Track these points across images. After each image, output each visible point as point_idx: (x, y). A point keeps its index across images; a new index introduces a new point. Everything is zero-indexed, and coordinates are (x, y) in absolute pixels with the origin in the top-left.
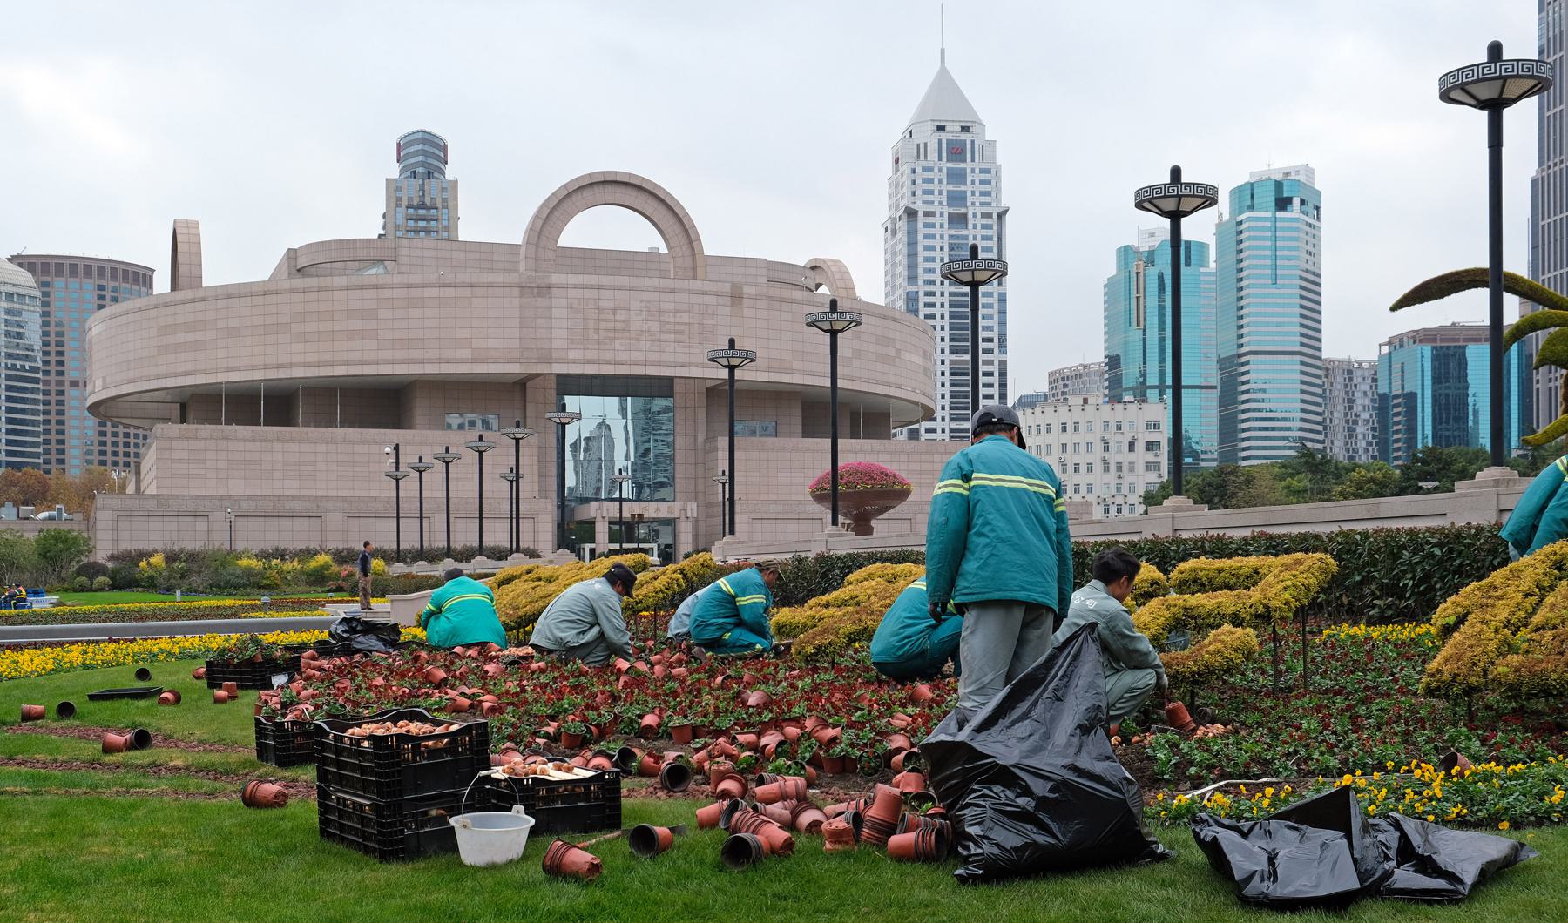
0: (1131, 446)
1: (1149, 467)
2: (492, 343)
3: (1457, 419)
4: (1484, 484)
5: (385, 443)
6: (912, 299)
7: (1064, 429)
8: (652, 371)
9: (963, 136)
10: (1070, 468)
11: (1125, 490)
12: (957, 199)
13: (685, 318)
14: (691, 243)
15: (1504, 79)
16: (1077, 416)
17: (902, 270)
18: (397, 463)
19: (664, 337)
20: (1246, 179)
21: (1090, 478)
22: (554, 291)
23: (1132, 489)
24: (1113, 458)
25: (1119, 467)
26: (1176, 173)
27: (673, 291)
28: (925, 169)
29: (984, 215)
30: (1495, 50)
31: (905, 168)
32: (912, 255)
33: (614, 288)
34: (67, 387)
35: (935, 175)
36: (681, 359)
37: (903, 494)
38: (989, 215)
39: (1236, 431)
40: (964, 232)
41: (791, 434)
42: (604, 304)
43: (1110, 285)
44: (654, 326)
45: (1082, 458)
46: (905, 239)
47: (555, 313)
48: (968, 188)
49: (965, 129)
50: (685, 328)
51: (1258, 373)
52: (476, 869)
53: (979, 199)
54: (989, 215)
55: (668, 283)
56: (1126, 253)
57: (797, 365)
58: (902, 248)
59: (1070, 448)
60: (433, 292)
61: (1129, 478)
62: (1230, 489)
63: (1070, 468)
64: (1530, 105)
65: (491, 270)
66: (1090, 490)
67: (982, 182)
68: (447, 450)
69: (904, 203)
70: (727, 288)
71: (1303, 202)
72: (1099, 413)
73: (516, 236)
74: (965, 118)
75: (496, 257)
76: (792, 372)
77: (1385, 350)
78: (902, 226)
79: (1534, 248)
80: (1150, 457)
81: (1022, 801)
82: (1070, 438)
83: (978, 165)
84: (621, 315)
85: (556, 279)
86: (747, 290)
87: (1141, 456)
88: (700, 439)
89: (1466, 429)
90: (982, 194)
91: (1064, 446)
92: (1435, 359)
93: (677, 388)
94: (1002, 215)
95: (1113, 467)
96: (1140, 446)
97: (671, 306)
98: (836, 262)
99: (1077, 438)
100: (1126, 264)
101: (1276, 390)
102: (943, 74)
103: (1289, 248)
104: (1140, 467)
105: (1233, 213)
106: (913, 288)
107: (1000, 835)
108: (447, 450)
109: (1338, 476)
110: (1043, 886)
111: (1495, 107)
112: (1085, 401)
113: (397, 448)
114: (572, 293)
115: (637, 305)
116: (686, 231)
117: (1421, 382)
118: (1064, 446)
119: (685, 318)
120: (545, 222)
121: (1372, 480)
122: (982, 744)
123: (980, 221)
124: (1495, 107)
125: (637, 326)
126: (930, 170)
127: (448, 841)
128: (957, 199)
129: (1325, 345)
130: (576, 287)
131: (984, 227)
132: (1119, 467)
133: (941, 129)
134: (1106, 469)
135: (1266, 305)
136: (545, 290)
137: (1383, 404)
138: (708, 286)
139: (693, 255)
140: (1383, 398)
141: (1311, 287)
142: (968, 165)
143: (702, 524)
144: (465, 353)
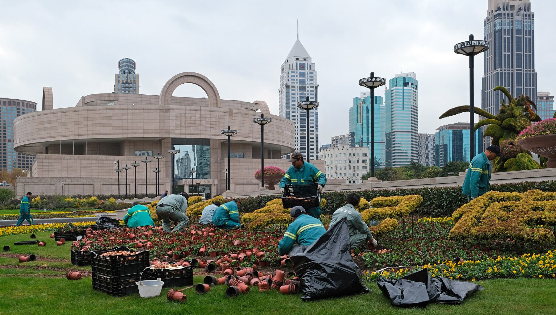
0: (358, 161)
1: (364, 168)
2: (150, 128)
3: (460, 153)
5: (114, 160)
7: (337, 156)
9: (304, 62)
10: (339, 168)
11: (356, 175)
13: (214, 120)
14: (216, 95)
15: (474, 46)
16: (341, 151)
17: (284, 104)
19: (207, 126)
20: (394, 76)
26: (372, 74)
27: (210, 111)
28: (292, 72)
30: (471, 37)
31: (286, 72)
32: (288, 100)
33: (190, 110)
34: (7, 142)
36: (212, 133)
38: (313, 87)
39: (391, 156)
40: (305, 93)
41: (248, 157)
42: (187, 115)
43: (351, 110)
44: (204, 122)
45: (342, 165)
46: (285, 95)
47: (171, 118)
48: (306, 79)
49: (305, 60)
50: (214, 123)
51: (398, 138)
53: (309, 82)
54: (313, 87)
56: (356, 99)
57: (250, 135)
58: (284, 98)
59: (338, 162)
60: (131, 111)
61: (357, 172)
63: (339, 168)
64: (482, 54)
65: (150, 104)
66: (345, 175)
67: (310, 77)
68: (135, 162)
69: (285, 83)
70: (228, 110)
71: (412, 84)
72: (348, 151)
73: (158, 93)
74: (305, 56)
75: (151, 100)
76: (248, 137)
77: (438, 131)
78: (285, 90)
79: (483, 99)
80: (364, 165)
81: (323, 274)
82: (338, 159)
84: (193, 119)
85: (171, 107)
86: (234, 111)
87: (361, 164)
88: (219, 159)
89: (462, 156)
90: (310, 80)
92: (453, 134)
93: (211, 142)
94: (317, 87)
95: (352, 168)
96: (361, 161)
97: (190, 115)
98: (263, 102)
99: (341, 158)
100: (357, 103)
101: (404, 143)
102: (298, 41)
103: (408, 99)
104: (361, 168)
105: (390, 87)
106: (288, 110)
107: (316, 285)
108: (135, 162)
111: (471, 55)
112: (343, 147)
113: (118, 162)
114: (177, 111)
115: (198, 116)
116: (214, 91)
117: (449, 141)
118: (337, 161)
119: (214, 120)
121: (434, 172)
124: (471, 55)
125: (198, 122)
126: (294, 72)
127: (136, 290)
129: (419, 129)
131: (311, 91)
133: (297, 59)
134: (350, 169)
137: (437, 148)
138: (221, 109)
139: (217, 99)
140: (437, 146)
142: (306, 71)
143: (219, 186)
144: (141, 131)
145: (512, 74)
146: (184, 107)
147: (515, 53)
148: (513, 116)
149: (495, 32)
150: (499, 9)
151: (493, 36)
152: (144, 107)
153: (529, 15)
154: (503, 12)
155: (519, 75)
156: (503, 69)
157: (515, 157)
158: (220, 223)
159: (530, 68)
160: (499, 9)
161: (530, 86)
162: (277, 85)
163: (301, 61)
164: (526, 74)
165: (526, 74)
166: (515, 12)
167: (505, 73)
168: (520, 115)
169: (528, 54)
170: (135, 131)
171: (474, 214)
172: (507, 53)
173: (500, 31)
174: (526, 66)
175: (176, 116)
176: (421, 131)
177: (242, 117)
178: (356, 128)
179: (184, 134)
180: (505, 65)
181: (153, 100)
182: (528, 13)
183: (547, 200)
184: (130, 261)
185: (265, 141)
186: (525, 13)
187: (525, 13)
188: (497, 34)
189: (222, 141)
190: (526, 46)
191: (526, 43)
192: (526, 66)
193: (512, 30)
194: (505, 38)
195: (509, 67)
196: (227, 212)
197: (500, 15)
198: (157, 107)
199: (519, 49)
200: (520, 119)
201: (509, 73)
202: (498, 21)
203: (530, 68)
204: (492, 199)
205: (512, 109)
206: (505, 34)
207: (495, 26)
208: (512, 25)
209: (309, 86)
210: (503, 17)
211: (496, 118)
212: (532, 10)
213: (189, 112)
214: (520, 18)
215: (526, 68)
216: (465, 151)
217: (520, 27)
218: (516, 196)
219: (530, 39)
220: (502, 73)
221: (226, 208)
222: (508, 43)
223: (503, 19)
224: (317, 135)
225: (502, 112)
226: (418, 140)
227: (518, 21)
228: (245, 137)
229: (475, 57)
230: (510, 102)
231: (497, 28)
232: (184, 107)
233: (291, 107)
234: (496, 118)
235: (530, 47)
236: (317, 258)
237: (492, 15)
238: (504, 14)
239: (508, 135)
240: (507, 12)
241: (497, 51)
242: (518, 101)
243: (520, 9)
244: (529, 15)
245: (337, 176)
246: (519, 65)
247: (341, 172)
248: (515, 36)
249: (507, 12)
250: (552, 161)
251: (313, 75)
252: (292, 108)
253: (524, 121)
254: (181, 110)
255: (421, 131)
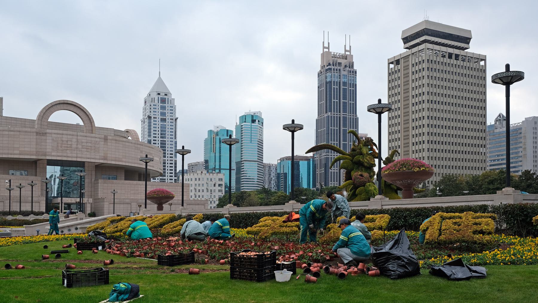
0: (215, 185)
1: (219, 191)
2: (26, 149)
3: (297, 180)
4: (376, 199)
5: (6, 179)
6: (149, 142)
7: (196, 180)
8: (79, 160)
9: (165, 97)
10: (197, 191)
11: (213, 197)
12: (163, 114)
13: (90, 145)
14: (91, 123)
15: (383, 108)
16: (200, 176)
17: (146, 133)
18: (10, 185)
19: (83, 150)
21: (203, 194)
22: (48, 135)
23: (215, 196)
24: (209, 189)
25: (211, 191)
26: (293, 121)
27: (86, 137)
28: (154, 105)
29: (171, 119)
30: (380, 101)
31: (148, 104)
32: (150, 129)
33: (67, 135)
35: (157, 107)
36: (88, 156)
37: (172, 198)
38: (172, 119)
39: (240, 182)
41: (121, 179)
42: (64, 139)
43: (206, 140)
44: (80, 147)
45: (201, 188)
46: (147, 125)
47: (48, 141)
48: (166, 111)
49: (166, 95)
50: (90, 148)
51: (246, 166)
52: (279, 282)
53: (169, 115)
54: (172, 119)
55: (85, 134)
56: (210, 132)
57: (123, 160)
58: (147, 127)
59: (197, 185)
60: (7, 133)
61: (213, 194)
62: (244, 197)
63: (197, 191)
64: (387, 113)
65: (25, 127)
66: (203, 197)
67: (171, 110)
68: (32, 182)
69: (147, 114)
70: (103, 136)
71: (259, 121)
72: (206, 176)
73: (35, 118)
74: (166, 92)
75: (26, 123)
76: (122, 161)
77: (279, 161)
78: (147, 121)
79: (317, 137)
80: (220, 188)
81: (402, 263)
82: (197, 182)
83: (169, 105)
84: (69, 143)
85: (48, 131)
86: (109, 137)
87: (217, 188)
88: (93, 180)
89: (299, 183)
90: (171, 113)
91: (196, 184)
93: (86, 165)
94: (176, 119)
95: (209, 191)
96: (217, 185)
97: (85, 141)
98: (134, 131)
99: (200, 182)
100: (211, 135)
101: (251, 171)
102: (160, 78)
103: (255, 133)
104: (217, 191)
105: (240, 123)
106: (150, 139)
107: (399, 270)
108: (32, 182)
109: (271, 195)
110: (409, 279)
111: (380, 114)
112: (202, 172)
113: (10, 181)
114: (53, 135)
115: (74, 140)
116: (90, 119)
117: (288, 170)
118: (196, 184)
119: (90, 145)
120: (44, 114)
121: (282, 196)
122: (391, 251)
123: (170, 121)
124: (380, 114)
125: (74, 146)
126: (156, 105)
127: (273, 277)
128: (163, 114)
129: (264, 159)
130: (55, 134)
131: (171, 122)
132: (211, 191)
133: (159, 94)
134: (208, 191)
135: (248, 148)
136: (45, 134)
137: (278, 176)
138: (97, 136)
139: (92, 126)
140: (278, 174)
141: (260, 144)
142: (166, 105)
143: (93, 205)
144: (18, 152)
145: (340, 117)
146: (61, 132)
147: (342, 101)
148: (361, 154)
149: (326, 83)
150: (329, 64)
151: (325, 86)
152: (21, 129)
153: (353, 72)
154: (333, 67)
155: (345, 119)
156: (333, 113)
157: (364, 186)
158: (216, 236)
159: (353, 114)
160: (329, 64)
161: (334, 127)
162: (141, 116)
163: (162, 95)
164: (350, 118)
165: (350, 118)
166: (342, 68)
167: (334, 117)
168: (367, 153)
169: (352, 102)
170: (10, 152)
171: (436, 227)
172: (336, 100)
173: (330, 82)
174: (350, 112)
175: (53, 140)
176: (265, 161)
177: (116, 143)
178: (210, 157)
179: (60, 156)
180: (334, 110)
181: (28, 123)
182: (352, 70)
183: (481, 218)
184: (268, 258)
185: (148, 167)
186: (350, 69)
187: (350, 69)
188: (328, 85)
189: (96, 164)
190: (350, 96)
191: (350, 94)
192: (350, 112)
193: (340, 82)
194: (334, 88)
195: (337, 112)
196: (221, 227)
197: (330, 69)
198: (34, 130)
199: (345, 98)
200: (366, 156)
201: (337, 117)
202: (329, 74)
203: (353, 114)
204: (443, 218)
205: (361, 149)
206: (334, 85)
207: (326, 78)
208: (340, 78)
209: (170, 118)
210: (333, 71)
211: (349, 155)
212: (355, 68)
213: (66, 136)
214: (346, 73)
215: (350, 113)
216: (302, 178)
217: (346, 80)
218: (458, 216)
219: (353, 104)
220: (331, 116)
221: (220, 224)
222: (337, 92)
223: (333, 73)
224: (176, 161)
225: (353, 150)
226: (262, 167)
227: (344, 75)
228: (119, 161)
229: (383, 115)
230: (359, 143)
231: (328, 80)
232: (61, 132)
233: (152, 135)
234: (349, 155)
235: (353, 97)
236: (396, 252)
237: (324, 69)
238: (334, 69)
239: (358, 169)
240: (336, 68)
241: (328, 99)
242: (365, 142)
243: (346, 66)
244: (353, 72)
245: (196, 197)
246: (345, 111)
247: (199, 194)
248: (342, 87)
249: (336, 68)
250: (406, 190)
251: (173, 109)
252: (154, 137)
253: (369, 158)
254: (58, 134)
255: (265, 161)
